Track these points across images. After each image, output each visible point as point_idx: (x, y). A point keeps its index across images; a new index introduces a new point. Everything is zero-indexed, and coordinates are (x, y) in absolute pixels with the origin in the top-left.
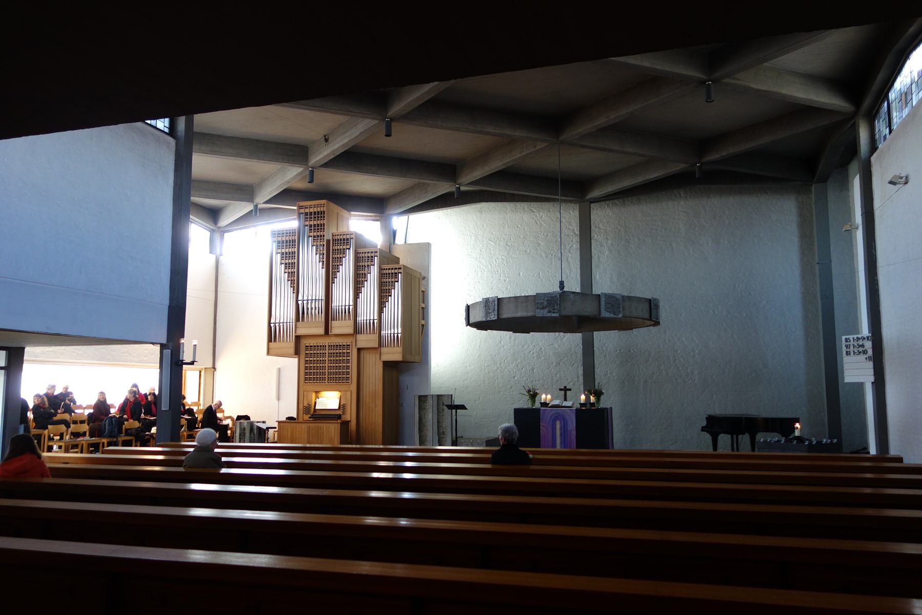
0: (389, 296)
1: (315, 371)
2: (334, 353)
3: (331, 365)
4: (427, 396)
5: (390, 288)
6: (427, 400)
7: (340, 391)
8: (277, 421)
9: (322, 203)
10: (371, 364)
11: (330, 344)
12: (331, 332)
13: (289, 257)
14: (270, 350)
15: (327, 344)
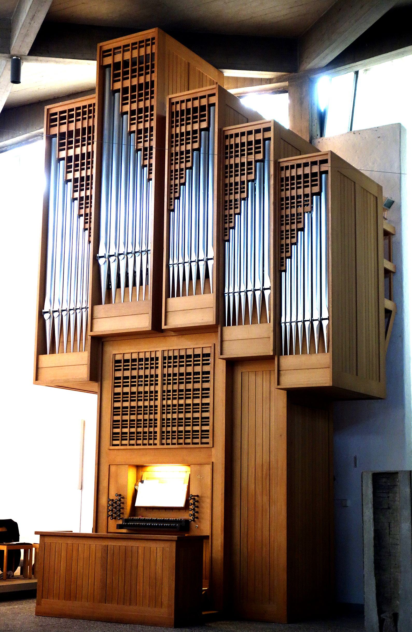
0: (299, 230)
1: (133, 417)
2: (175, 375)
3: (170, 402)
4: (396, 473)
5: (301, 210)
6: (395, 485)
7: (189, 466)
8: (36, 533)
9: (150, 37)
10: (259, 396)
11: (166, 355)
12: (166, 324)
13: (83, 164)
14: (41, 372)
15: (159, 355)
